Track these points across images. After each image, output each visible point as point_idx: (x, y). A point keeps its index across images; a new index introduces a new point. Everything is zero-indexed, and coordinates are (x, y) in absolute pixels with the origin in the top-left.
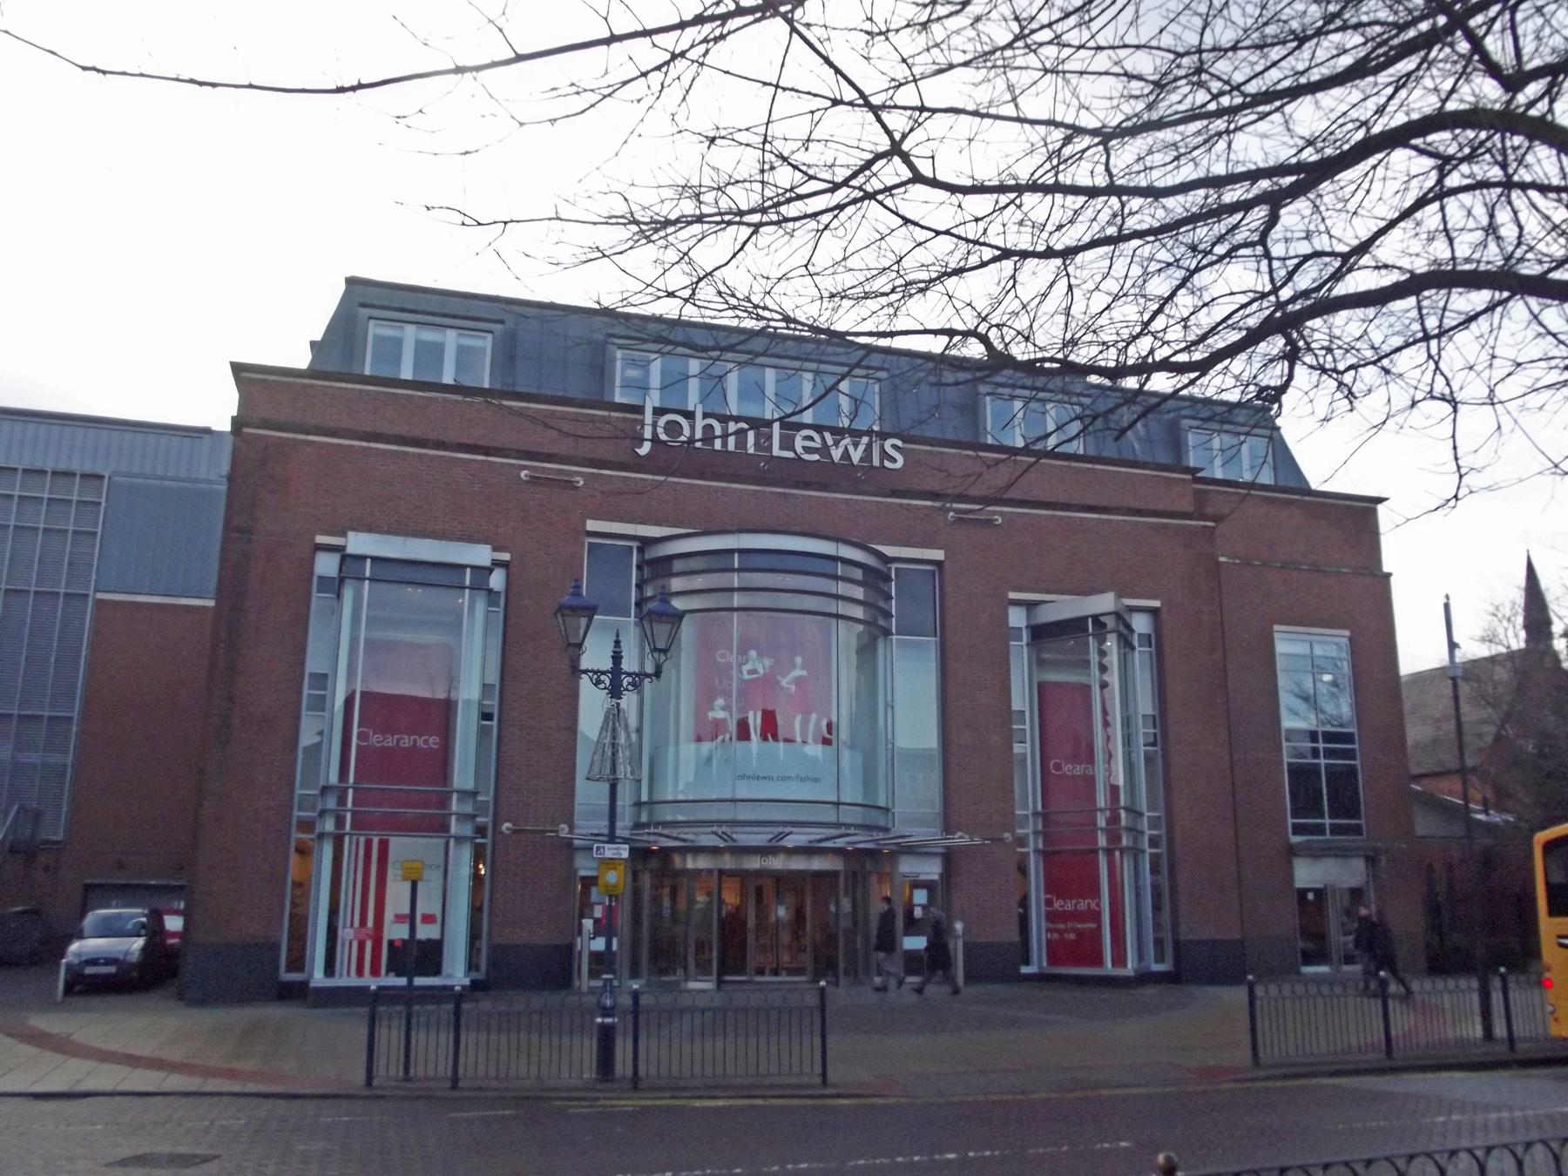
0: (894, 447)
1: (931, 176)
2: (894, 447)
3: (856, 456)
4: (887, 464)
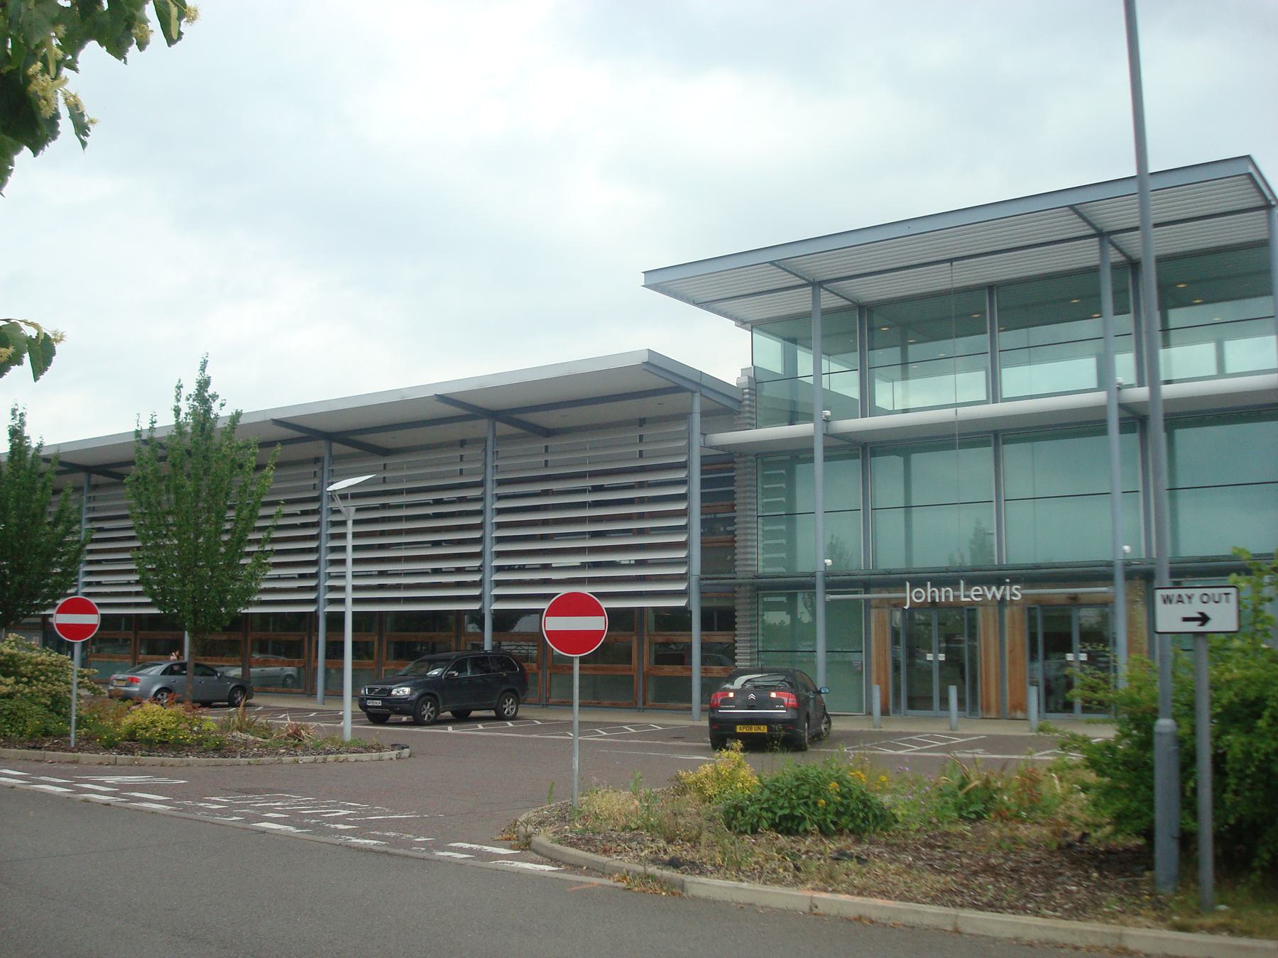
0: (1016, 589)
1: (497, 423)
2: (1016, 589)
4: (1014, 598)
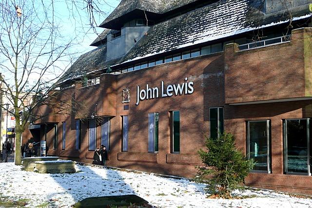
4: (189, 92)
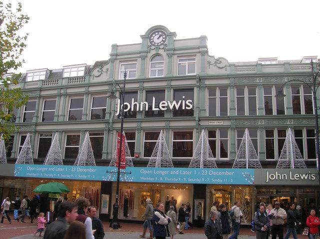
3: (306, 178)
4: (187, 108)
